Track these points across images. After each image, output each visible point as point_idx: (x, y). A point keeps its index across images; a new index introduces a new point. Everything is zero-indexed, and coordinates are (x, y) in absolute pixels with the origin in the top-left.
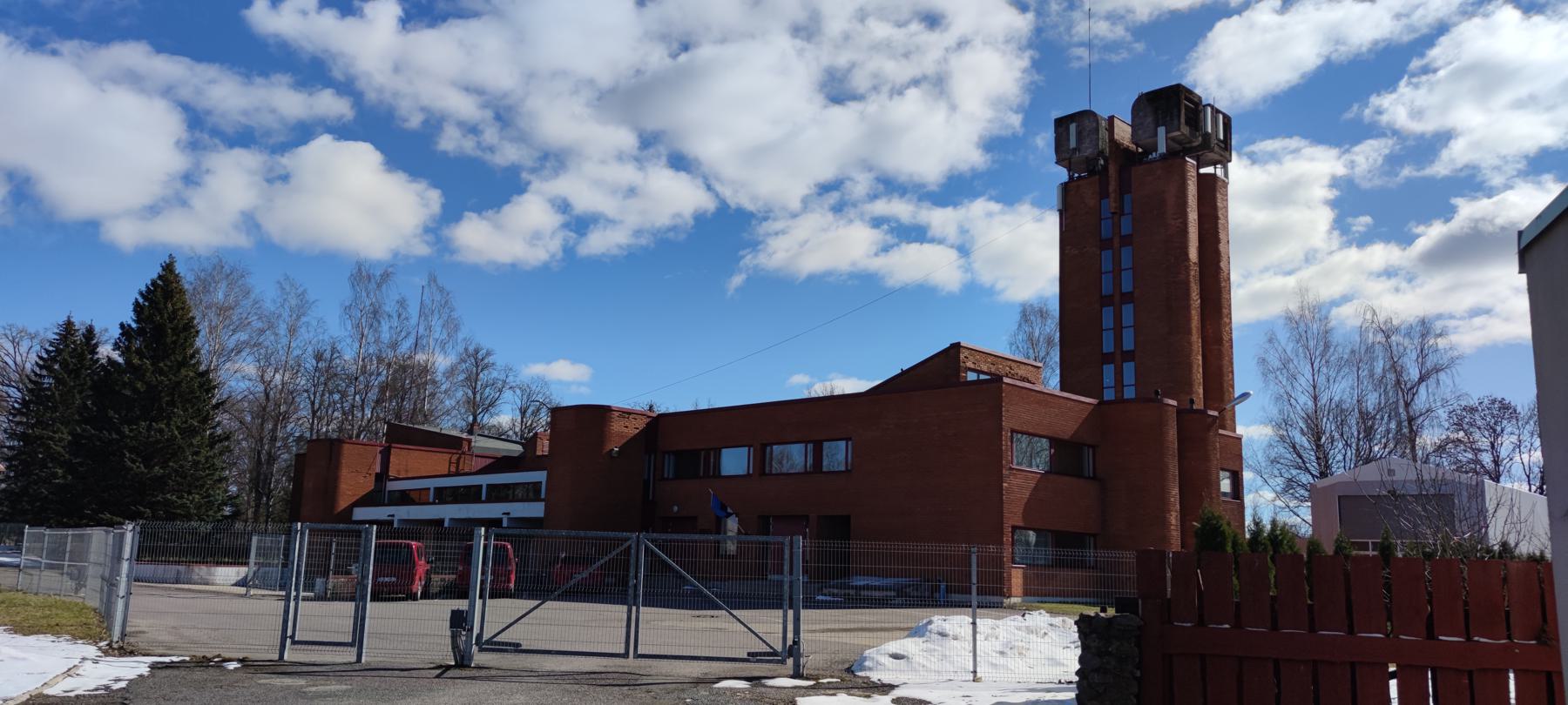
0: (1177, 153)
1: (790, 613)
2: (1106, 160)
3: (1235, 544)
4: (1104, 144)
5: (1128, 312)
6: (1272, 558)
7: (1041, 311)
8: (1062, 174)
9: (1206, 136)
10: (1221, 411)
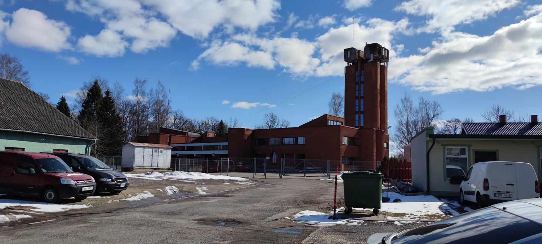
0: (376, 60)
4: (357, 57)
5: (362, 101)
6: (395, 238)
8: (346, 64)
9: (383, 56)
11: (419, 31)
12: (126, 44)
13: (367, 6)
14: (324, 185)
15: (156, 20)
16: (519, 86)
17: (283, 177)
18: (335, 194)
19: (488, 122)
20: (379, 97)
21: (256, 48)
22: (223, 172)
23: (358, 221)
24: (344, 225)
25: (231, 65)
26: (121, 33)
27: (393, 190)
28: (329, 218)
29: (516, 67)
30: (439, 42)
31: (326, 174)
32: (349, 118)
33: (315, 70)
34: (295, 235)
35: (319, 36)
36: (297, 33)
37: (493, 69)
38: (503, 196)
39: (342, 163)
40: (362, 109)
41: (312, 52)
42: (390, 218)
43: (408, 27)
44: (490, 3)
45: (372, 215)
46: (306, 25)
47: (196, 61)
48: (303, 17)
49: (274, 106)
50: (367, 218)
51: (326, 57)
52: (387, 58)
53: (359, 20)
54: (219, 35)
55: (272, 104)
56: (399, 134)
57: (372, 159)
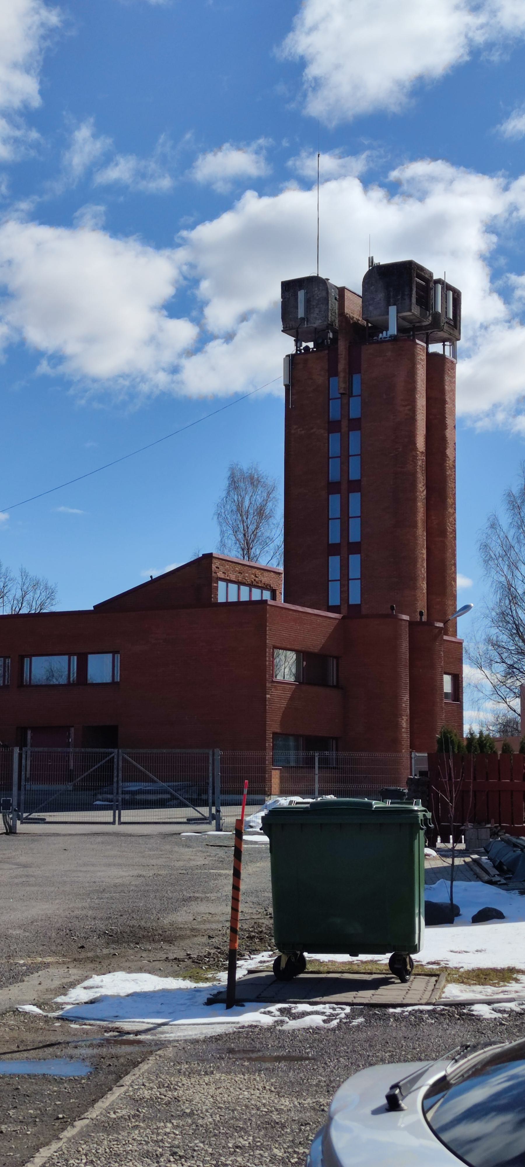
0: (410, 331)
1: (117, 812)
2: (335, 332)
3: (459, 747)
4: (333, 317)
5: (355, 499)
6: (441, 1086)
7: (252, 478)
8: (288, 345)
9: (436, 317)
10: (445, 622)
13: (394, 109)
14: (196, 858)
17: (20, 827)
18: (235, 899)
23: (327, 1009)
24: (270, 1029)
27: (473, 872)
28: (210, 1002)
31: (205, 811)
32: (303, 573)
34: (59, 1081)
35: (192, 227)
36: (101, 208)
39: (274, 762)
41: (167, 291)
42: (454, 992)
45: (385, 982)
46: (141, 175)
50: (366, 996)
51: (221, 314)
52: (456, 323)
53: (359, 164)
56: (504, 638)
57: (394, 744)
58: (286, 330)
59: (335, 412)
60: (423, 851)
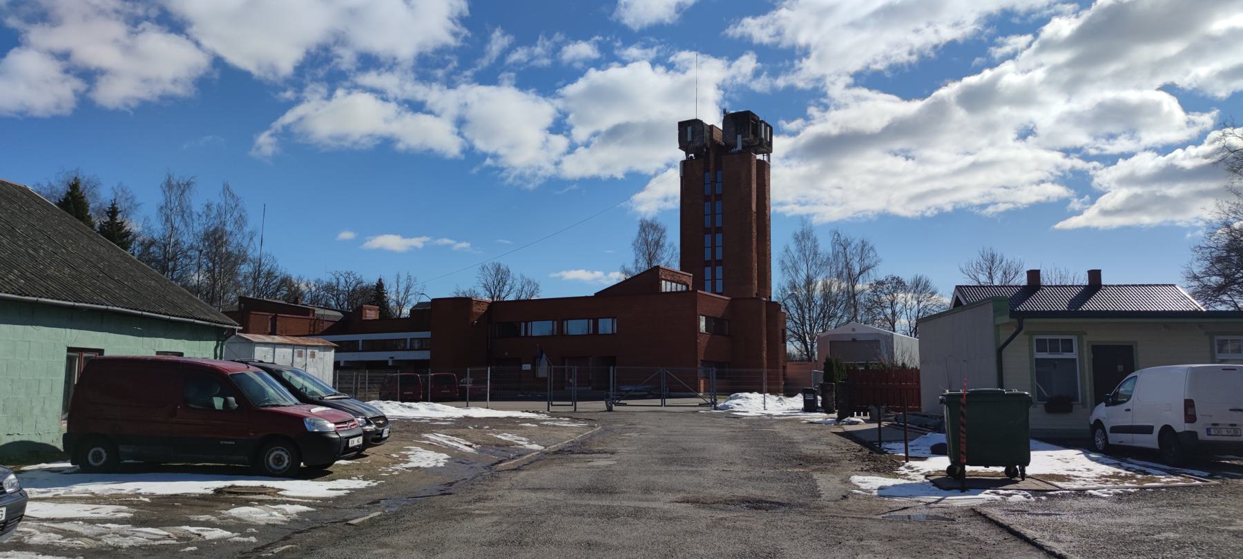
5: (719, 237)
11: (781, 82)
12: (79, 84)
13: (668, 20)
15: (157, 27)
16: (983, 206)
17: (615, 408)
19: (975, 284)
20: (754, 230)
21: (417, 107)
22: (471, 400)
25: (355, 143)
26: (64, 56)
29: (975, 166)
30: (822, 108)
33: (557, 164)
35: (565, 85)
36: (513, 74)
37: (932, 170)
38: (1224, 432)
40: (719, 256)
43: (757, 74)
44: (922, 26)
47: (267, 133)
48: (525, 38)
49: (464, 245)
51: (581, 133)
53: (652, 53)
54: (321, 73)
55: (459, 241)
57: (761, 366)
58: (681, 147)
59: (708, 191)
60: (948, 438)
